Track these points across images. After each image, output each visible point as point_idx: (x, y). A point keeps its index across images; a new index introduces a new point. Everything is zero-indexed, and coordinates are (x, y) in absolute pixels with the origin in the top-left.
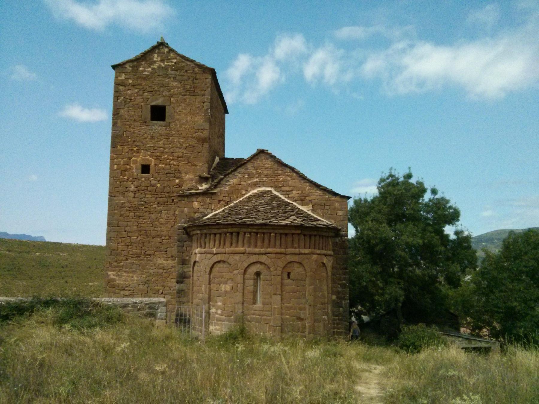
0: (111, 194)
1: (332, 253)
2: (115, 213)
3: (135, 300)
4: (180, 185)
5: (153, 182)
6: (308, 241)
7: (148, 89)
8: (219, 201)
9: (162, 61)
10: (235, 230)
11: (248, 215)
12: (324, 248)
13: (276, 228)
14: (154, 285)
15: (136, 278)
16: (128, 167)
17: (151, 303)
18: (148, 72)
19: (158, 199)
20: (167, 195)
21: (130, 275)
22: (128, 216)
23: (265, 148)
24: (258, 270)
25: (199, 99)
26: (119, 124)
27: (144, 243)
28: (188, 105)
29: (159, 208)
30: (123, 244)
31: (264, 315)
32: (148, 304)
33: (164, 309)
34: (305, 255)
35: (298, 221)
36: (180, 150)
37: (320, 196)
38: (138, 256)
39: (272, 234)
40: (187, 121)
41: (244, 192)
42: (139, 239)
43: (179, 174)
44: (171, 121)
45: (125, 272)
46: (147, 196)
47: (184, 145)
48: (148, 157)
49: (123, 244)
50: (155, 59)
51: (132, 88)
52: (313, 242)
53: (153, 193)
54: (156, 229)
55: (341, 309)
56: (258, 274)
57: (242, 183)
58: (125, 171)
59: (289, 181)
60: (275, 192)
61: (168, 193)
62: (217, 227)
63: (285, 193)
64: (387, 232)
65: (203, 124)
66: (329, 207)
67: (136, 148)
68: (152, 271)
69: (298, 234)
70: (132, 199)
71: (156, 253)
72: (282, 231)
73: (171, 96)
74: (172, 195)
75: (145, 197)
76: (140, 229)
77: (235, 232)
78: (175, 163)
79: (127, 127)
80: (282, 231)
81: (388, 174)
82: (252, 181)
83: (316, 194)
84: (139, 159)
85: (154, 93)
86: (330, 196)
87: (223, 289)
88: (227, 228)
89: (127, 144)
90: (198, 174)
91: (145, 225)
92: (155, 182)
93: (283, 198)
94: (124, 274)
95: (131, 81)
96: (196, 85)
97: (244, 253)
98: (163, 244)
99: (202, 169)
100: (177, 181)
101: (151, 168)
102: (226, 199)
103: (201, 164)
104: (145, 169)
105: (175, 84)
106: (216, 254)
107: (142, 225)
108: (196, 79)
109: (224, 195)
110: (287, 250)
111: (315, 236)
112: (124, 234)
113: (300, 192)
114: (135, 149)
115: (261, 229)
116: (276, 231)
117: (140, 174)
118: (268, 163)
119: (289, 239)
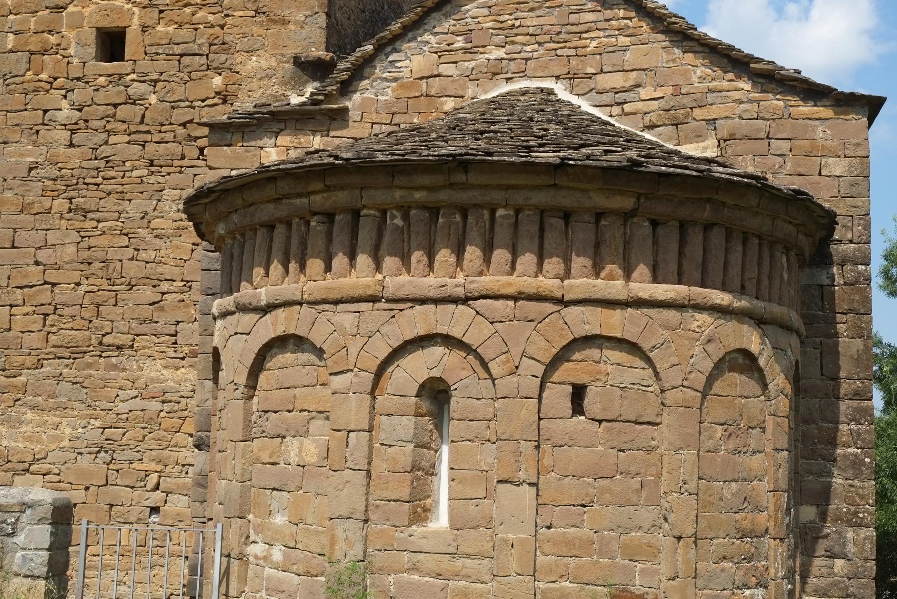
1: (795, 319)
4: (224, 97)
5: (136, 89)
6: (674, 247)
10: (341, 198)
12: (749, 286)
13: (513, 181)
14: (129, 455)
15: (68, 431)
16: (53, 39)
19: (149, 147)
20: (181, 131)
21: (51, 419)
24: (435, 373)
27: (98, 306)
29: (153, 179)
30: (26, 309)
31: (457, 575)
34: (652, 312)
37: (750, 101)
38: (76, 353)
39: (500, 212)
42: (83, 288)
43: (223, 57)
45: (33, 408)
46: (112, 139)
49: (26, 309)
53: (133, 128)
54: (143, 255)
55: (839, 563)
56: (436, 394)
57: (444, 69)
58: (44, 52)
59: (625, 48)
61: (184, 125)
62: (270, 191)
63: (607, 98)
66: (786, 145)
68: (123, 407)
69: (627, 216)
70: (62, 150)
72: (541, 198)
75: (106, 143)
76: (86, 255)
77: (344, 211)
78: (211, 18)
80: (541, 198)
82: (482, 58)
83: (736, 95)
86: (793, 100)
90: (290, 52)
91: (102, 241)
94: (30, 415)
97: (373, 299)
100: (218, 81)
101: (128, 38)
103: (300, 17)
104: (111, 44)
106: (270, 308)
107: (93, 242)
109: (374, 117)
112: (34, 274)
113: (669, 90)
115: (452, 186)
116: (519, 198)
119: (582, 231)
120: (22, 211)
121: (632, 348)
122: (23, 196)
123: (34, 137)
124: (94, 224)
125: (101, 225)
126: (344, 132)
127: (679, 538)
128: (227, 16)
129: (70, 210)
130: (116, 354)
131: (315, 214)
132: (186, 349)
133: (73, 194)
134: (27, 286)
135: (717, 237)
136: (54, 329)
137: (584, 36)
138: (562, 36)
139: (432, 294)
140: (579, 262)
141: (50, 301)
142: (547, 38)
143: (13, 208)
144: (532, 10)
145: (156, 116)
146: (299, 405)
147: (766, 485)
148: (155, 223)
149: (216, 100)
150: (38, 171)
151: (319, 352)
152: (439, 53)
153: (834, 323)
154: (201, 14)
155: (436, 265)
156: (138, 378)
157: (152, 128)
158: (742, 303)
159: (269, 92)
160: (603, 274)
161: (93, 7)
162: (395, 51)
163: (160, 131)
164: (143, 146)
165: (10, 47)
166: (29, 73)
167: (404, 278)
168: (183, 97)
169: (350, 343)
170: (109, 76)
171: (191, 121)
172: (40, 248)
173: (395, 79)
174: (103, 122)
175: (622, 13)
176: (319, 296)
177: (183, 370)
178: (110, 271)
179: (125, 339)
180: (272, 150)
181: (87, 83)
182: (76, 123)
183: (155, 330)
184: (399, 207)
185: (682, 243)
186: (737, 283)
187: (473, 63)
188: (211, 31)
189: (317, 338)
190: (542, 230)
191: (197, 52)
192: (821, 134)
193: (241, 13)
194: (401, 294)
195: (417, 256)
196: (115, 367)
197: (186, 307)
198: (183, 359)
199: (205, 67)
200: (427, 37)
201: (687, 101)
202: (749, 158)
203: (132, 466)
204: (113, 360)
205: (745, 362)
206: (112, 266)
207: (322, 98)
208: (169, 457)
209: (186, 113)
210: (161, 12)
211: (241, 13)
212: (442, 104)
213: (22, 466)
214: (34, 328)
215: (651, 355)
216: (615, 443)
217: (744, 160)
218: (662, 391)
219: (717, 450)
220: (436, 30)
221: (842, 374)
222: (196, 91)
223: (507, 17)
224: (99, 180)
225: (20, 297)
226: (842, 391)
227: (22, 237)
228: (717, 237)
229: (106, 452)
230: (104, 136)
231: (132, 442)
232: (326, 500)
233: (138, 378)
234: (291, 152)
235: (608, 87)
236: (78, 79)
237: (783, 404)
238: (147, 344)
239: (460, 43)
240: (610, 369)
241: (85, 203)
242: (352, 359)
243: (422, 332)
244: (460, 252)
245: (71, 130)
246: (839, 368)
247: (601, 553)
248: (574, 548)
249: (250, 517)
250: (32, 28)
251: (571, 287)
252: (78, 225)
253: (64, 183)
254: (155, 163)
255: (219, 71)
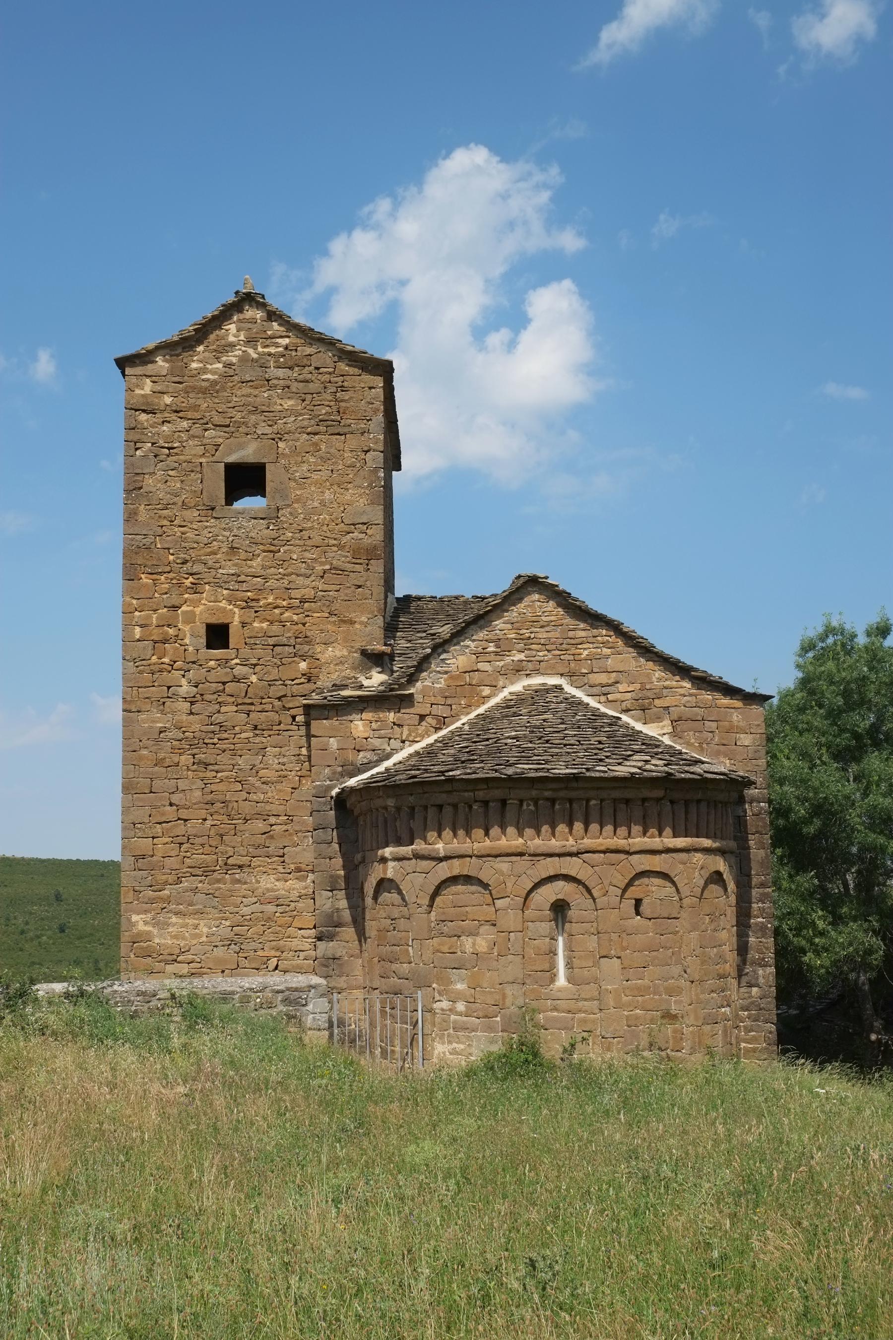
0: (128, 707)
2: (141, 758)
3: (247, 982)
5: (240, 670)
6: (683, 816)
7: (217, 419)
8: (422, 717)
9: (251, 341)
10: (498, 793)
11: (525, 755)
14: (253, 945)
15: (205, 930)
16: (171, 631)
17: (288, 989)
18: (213, 372)
20: (277, 703)
21: (191, 921)
22: (177, 765)
23: (529, 570)
24: (560, 897)
25: (353, 442)
26: (143, 514)
27: (221, 836)
28: (324, 460)
29: (257, 740)
32: (282, 992)
33: (323, 1003)
34: (674, 855)
35: (657, 767)
36: (307, 582)
37: (691, 695)
38: (207, 872)
39: (593, 802)
40: (323, 503)
41: (486, 691)
42: (209, 823)
44: (280, 503)
45: (176, 914)
46: (223, 709)
47: (319, 568)
48: (223, 604)
50: (231, 339)
51: (174, 416)
52: (693, 816)
53: (240, 701)
55: (755, 990)
56: (560, 908)
57: (481, 666)
58: (165, 641)
59: (607, 657)
60: (569, 689)
61: (279, 699)
62: (448, 787)
63: (595, 690)
64: (833, 781)
65: (368, 509)
66: (714, 725)
67: (191, 579)
69: (658, 800)
70: (184, 717)
71: (256, 862)
72: (616, 794)
73: (280, 436)
74: (291, 705)
75: (219, 712)
76: (209, 797)
78: (295, 617)
79: (165, 522)
81: (821, 630)
82: (508, 660)
83: (682, 691)
84: (198, 610)
85: (232, 429)
86: (718, 695)
87: (468, 948)
88: (473, 791)
89: (168, 569)
90: (358, 645)
91: (222, 787)
92: (245, 670)
93: (593, 703)
94: (174, 919)
95: (168, 400)
96: (342, 404)
97: (521, 854)
98: (272, 837)
99: (369, 631)
100: (303, 665)
101: (231, 631)
102: (439, 710)
103: (364, 619)
104: (217, 635)
105: (289, 403)
106: (447, 858)
107: (213, 787)
108: (343, 389)
109: (433, 700)
110: (630, 840)
111: (699, 801)
113: (638, 686)
114: (188, 582)
115: (566, 788)
117: (204, 650)
118: (551, 609)
120: (156, 765)
121: (665, 876)
122: (156, 753)
123: (162, 707)
124: (214, 774)
125: (219, 775)
126: (412, 710)
127: (692, 982)
128: (308, 616)
129: (194, 763)
130: (239, 871)
131: (476, 801)
132: (292, 867)
133: (195, 751)
134: (165, 822)
135: (703, 806)
136: (188, 854)
137: (580, 646)
138: (564, 646)
139: (557, 851)
140: (636, 829)
141: (184, 833)
142: (554, 647)
143: (149, 763)
144: (542, 627)
145: (257, 691)
146: (470, 917)
147: (726, 948)
148: (262, 773)
149: (302, 680)
150: (167, 733)
151: (486, 886)
152: (477, 654)
153: (747, 840)
154: (287, 614)
155: (557, 834)
156: (257, 889)
157: (254, 701)
158: (716, 845)
159: (343, 674)
160: (648, 834)
161: (202, 607)
162: (445, 652)
163: (261, 703)
164: (248, 715)
165: (137, 637)
166: (154, 657)
167: (537, 841)
168: (277, 678)
169: (507, 881)
170: (218, 660)
171: (285, 696)
172: (173, 793)
173: (446, 673)
174: (216, 696)
175: (604, 632)
176: (484, 852)
177: (290, 882)
178: (230, 809)
179: (245, 860)
180: (360, 723)
181: (201, 665)
182: (194, 697)
183: (268, 853)
184: (532, 799)
185: (687, 813)
186: (713, 834)
187: (502, 663)
188: (296, 627)
189: (483, 876)
190: (615, 811)
191: (286, 643)
192: (736, 718)
193: (319, 615)
194: (539, 851)
195: (545, 828)
196: (238, 881)
197: (290, 835)
198: (290, 873)
199: (293, 655)
200: (468, 642)
201: (650, 694)
202: (691, 733)
203: (258, 953)
204: (237, 876)
205: (717, 878)
206: (230, 805)
207: (396, 686)
208: (285, 946)
209: (280, 690)
210: (256, 612)
211: (319, 615)
212: (481, 691)
213: (171, 958)
214: (173, 853)
215: (675, 879)
216: (658, 931)
217: (688, 735)
218: (681, 900)
219: (707, 930)
220: (474, 637)
221: (753, 872)
222: (286, 673)
223: (525, 631)
224: (216, 741)
225: (159, 830)
226: (753, 883)
227: (157, 784)
228: (703, 806)
229: (235, 944)
230: (217, 706)
231: (255, 936)
232: (496, 973)
233: (257, 889)
234: (373, 724)
235: (597, 683)
236: (194, 663)
237: (733, 899)
238: (262, 864)
239: (492, 648)
240: (654, 889)
241: (206, 758)
242: (509, 890)
243: (552, 874)
244: (570, 825)
245: (191, 702)
246: (751, 869)
247: (655, 994)
248: (641, 991)
249: (434, 985)
250: (154, 622)
251: (634, 844)
252: (201, 775)
253: (188, 743)
254: (259, 727)
255: (303, 658)
